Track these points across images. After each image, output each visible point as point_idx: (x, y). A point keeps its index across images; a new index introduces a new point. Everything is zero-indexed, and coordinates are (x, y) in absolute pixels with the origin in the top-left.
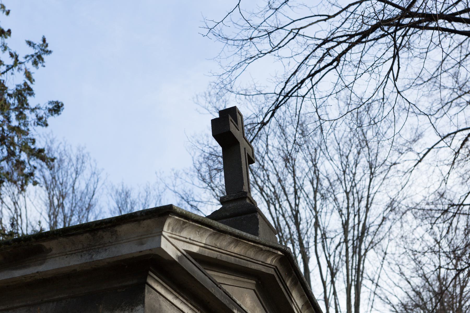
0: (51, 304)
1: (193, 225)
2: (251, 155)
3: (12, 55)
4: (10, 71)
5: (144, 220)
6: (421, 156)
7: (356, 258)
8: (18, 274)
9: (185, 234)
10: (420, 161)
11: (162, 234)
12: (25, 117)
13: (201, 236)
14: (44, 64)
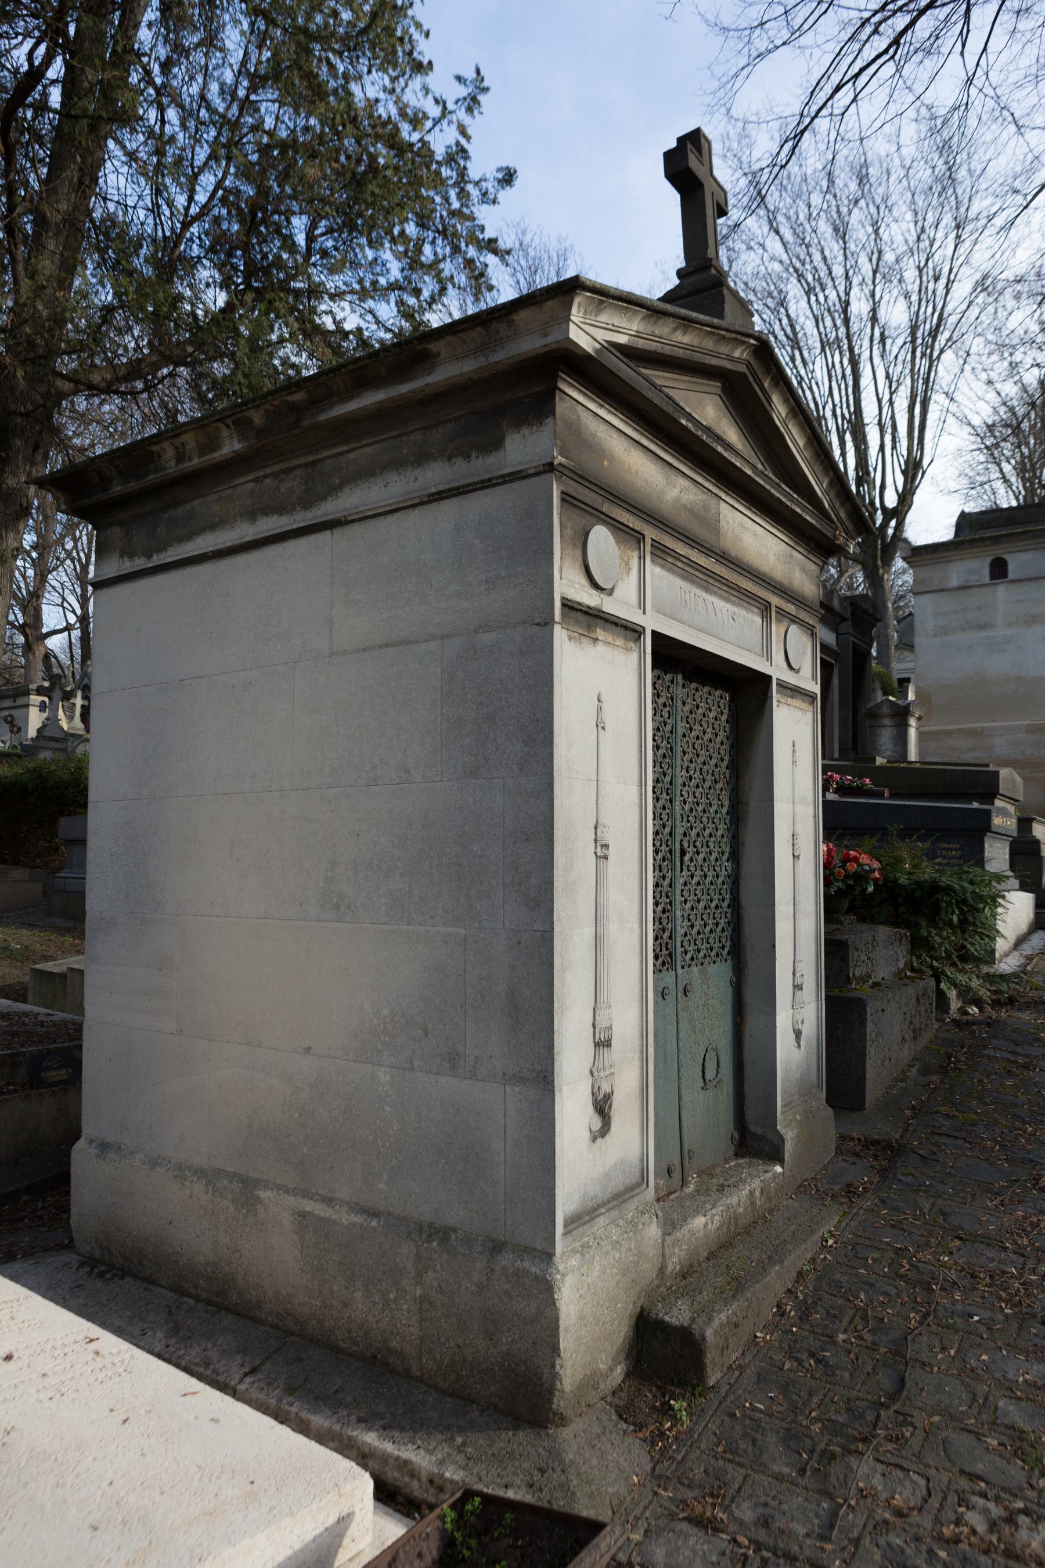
0: (448, 425)
1: (616, 305)
2: (722, 203)
3: (437, 101)
4: (439, 126)
5: (546, 301)
6: (1029, 198)
7: (925, 362)
8: (405, 388)
9: (604, 317)
10: (1026, 207)
11: (570, 320)
12: (468, 194)
13: (630, 320)
14: (482, 110)
